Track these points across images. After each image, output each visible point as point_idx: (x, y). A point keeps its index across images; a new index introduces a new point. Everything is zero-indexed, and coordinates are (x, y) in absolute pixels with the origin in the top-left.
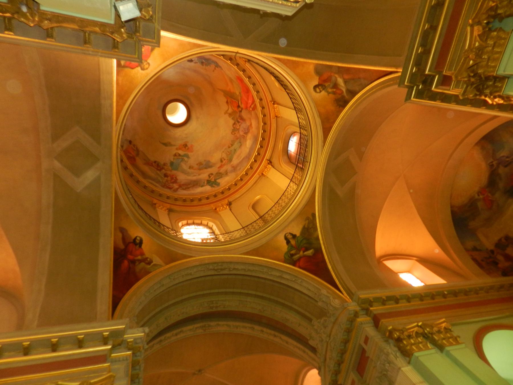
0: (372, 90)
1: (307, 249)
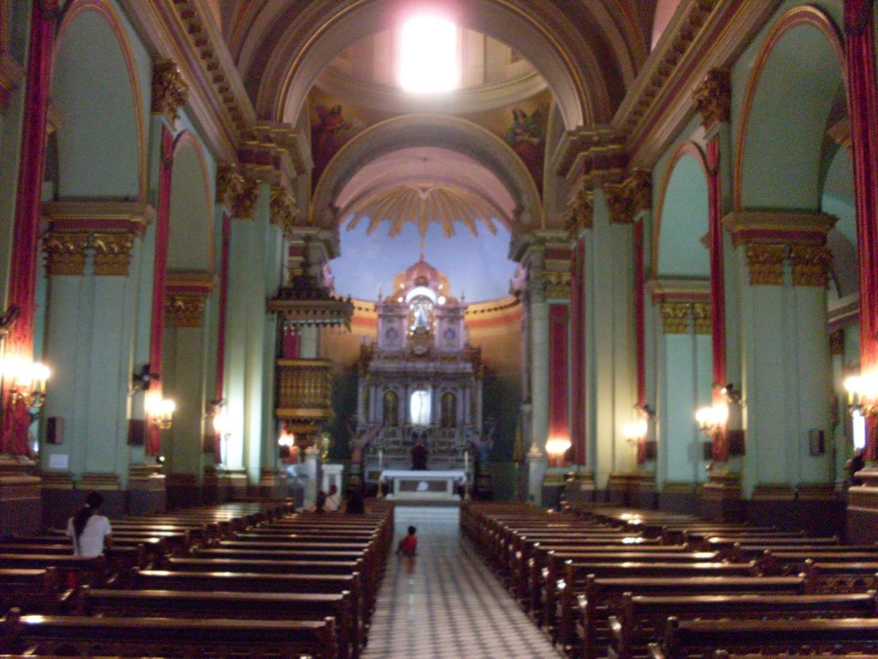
1: (533, 135)
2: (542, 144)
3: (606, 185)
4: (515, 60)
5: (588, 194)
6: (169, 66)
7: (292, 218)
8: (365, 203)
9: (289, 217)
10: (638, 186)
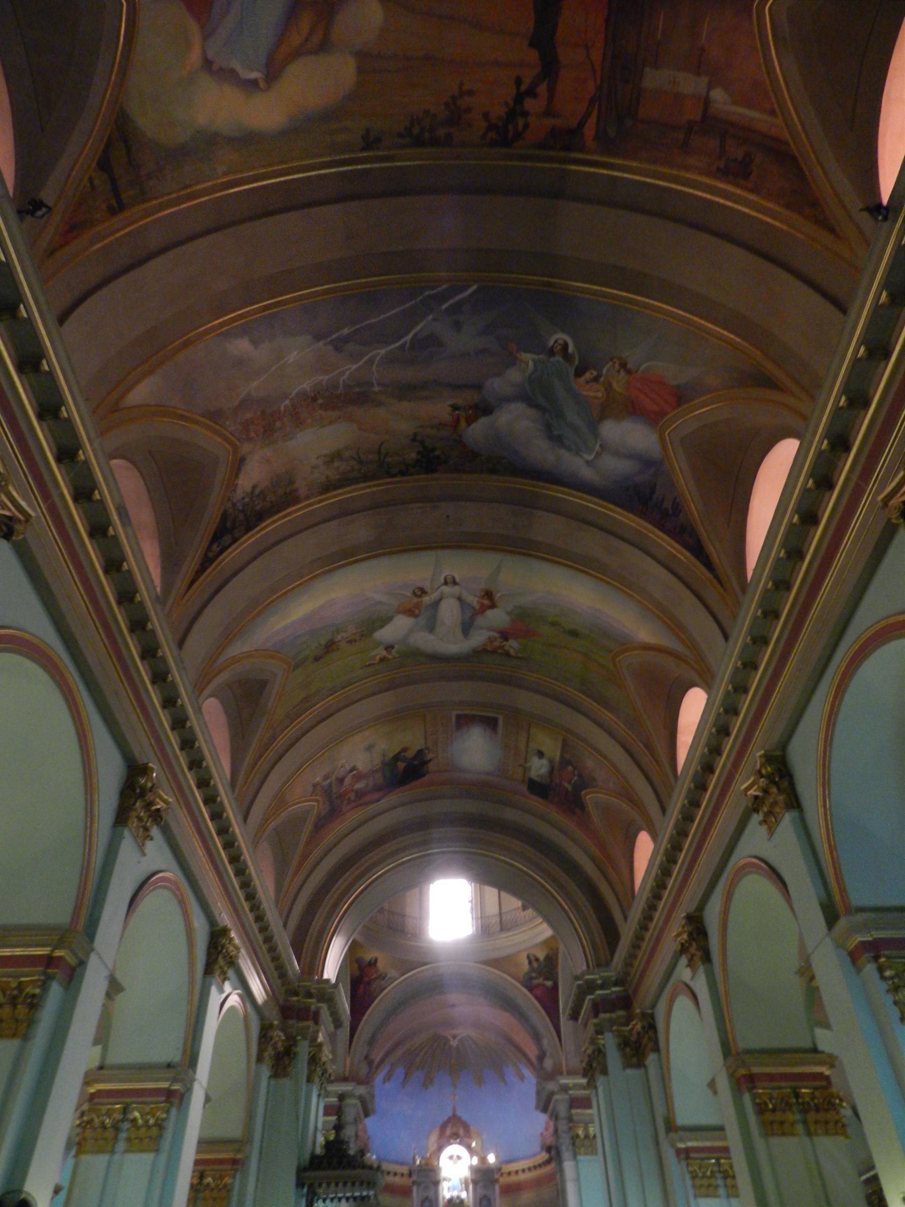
0: (176, 205)
1: (547, 979)
2: (555, 987)
3: (614, 1028)
4: (524, 908)
5: (599, 1039)
6: (225, 931)
7: (328, 1075)
8: (399, 1052)
9: (325, 1074)
10: (643, 1027)
